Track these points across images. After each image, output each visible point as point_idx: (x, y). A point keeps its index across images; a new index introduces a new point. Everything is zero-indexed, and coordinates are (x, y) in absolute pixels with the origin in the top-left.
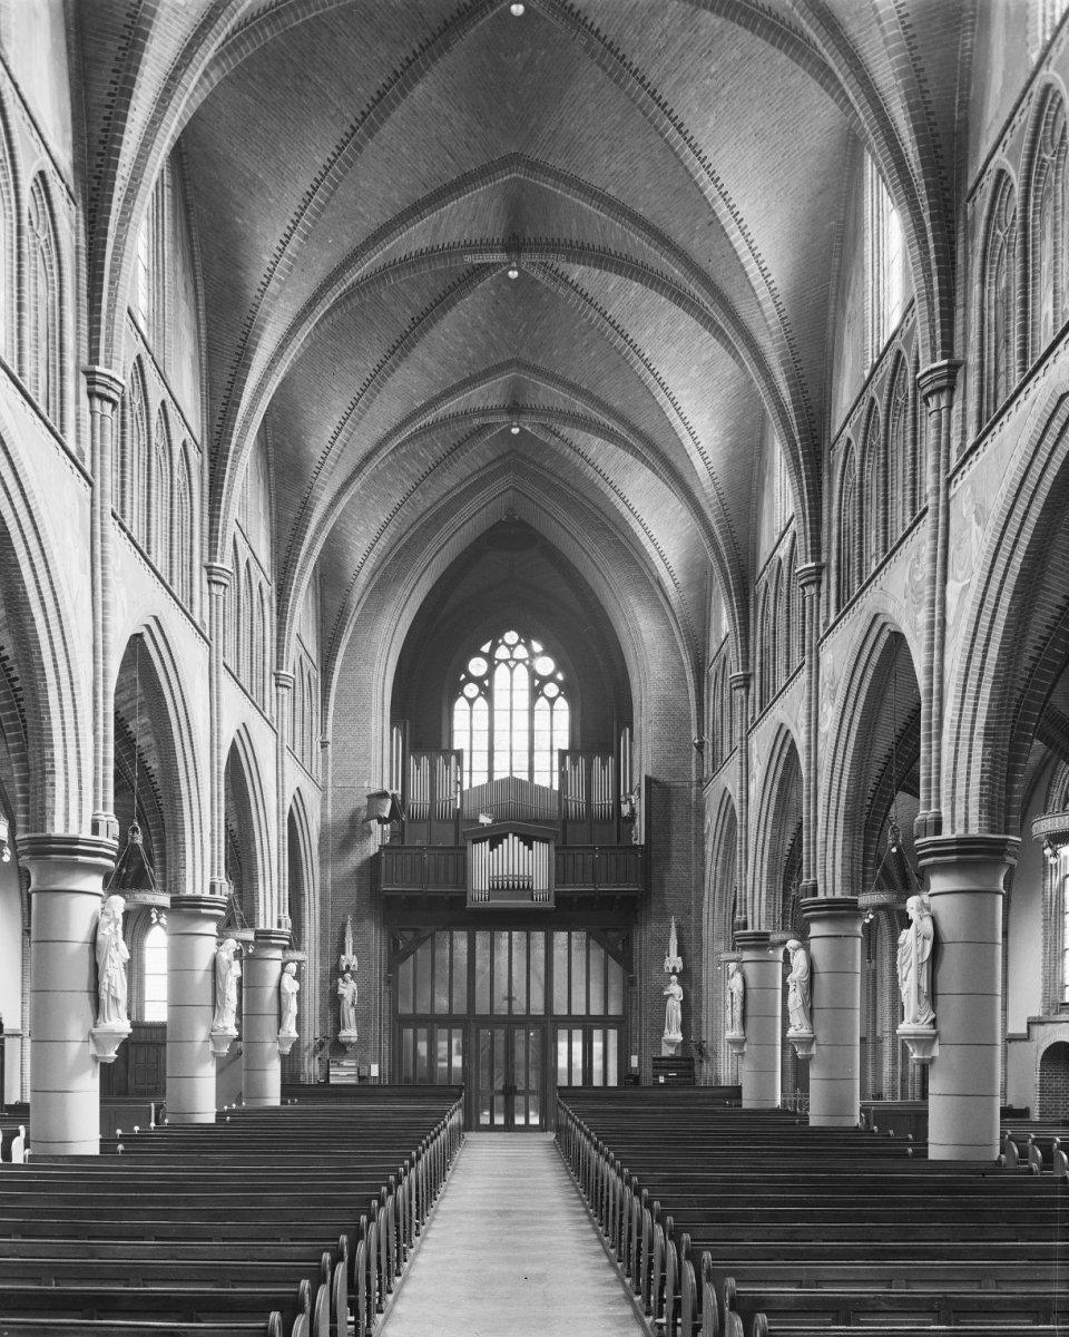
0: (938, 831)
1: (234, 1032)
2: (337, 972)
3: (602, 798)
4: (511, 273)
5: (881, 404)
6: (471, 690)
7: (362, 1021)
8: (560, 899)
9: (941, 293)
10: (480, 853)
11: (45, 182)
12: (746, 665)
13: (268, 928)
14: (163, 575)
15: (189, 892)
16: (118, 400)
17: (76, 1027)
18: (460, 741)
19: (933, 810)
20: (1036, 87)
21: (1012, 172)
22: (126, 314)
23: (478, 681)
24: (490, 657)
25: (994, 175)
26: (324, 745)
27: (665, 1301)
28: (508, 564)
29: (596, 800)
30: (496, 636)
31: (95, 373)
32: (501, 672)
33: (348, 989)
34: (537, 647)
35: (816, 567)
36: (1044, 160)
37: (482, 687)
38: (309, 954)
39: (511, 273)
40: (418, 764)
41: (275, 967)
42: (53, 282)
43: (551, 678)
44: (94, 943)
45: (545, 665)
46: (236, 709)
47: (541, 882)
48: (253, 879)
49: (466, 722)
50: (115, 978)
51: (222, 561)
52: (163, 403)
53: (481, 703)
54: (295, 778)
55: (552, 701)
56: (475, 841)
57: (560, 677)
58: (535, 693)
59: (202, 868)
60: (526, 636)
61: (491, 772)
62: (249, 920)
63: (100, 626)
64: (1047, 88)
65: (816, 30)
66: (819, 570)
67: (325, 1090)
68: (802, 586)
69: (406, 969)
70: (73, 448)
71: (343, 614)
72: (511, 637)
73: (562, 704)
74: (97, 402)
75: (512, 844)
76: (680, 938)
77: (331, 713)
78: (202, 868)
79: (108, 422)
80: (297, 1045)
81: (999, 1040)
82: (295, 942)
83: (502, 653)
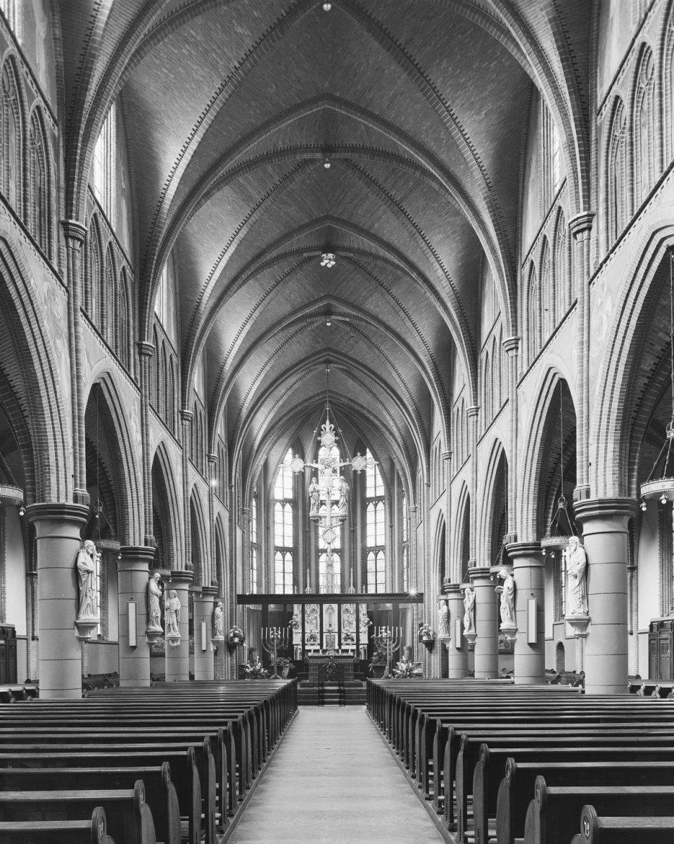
0: (516, 541)
4: (325, 6)
5: (537, 265)
9: (582, 171)
12: (476, 401)
13: (180, 570)
14: (97, 327)
16: (83, 239)
19: (585, 484)
21: (623, 96)
22: (87, 188)
25: (612, 99)
35: (587, 215)
36: (641, 88)
39: (325, 6)
42: (19, 127)
46: (158, 434)
48: (169, 539)
52: (110, 243)
63: (76, 378)
64: (644, 44)
65: (505, 16)
66: (477, 409)
68: (507, 351)
70: (56, 269)
74: (70, 240)
79: (77, 254)
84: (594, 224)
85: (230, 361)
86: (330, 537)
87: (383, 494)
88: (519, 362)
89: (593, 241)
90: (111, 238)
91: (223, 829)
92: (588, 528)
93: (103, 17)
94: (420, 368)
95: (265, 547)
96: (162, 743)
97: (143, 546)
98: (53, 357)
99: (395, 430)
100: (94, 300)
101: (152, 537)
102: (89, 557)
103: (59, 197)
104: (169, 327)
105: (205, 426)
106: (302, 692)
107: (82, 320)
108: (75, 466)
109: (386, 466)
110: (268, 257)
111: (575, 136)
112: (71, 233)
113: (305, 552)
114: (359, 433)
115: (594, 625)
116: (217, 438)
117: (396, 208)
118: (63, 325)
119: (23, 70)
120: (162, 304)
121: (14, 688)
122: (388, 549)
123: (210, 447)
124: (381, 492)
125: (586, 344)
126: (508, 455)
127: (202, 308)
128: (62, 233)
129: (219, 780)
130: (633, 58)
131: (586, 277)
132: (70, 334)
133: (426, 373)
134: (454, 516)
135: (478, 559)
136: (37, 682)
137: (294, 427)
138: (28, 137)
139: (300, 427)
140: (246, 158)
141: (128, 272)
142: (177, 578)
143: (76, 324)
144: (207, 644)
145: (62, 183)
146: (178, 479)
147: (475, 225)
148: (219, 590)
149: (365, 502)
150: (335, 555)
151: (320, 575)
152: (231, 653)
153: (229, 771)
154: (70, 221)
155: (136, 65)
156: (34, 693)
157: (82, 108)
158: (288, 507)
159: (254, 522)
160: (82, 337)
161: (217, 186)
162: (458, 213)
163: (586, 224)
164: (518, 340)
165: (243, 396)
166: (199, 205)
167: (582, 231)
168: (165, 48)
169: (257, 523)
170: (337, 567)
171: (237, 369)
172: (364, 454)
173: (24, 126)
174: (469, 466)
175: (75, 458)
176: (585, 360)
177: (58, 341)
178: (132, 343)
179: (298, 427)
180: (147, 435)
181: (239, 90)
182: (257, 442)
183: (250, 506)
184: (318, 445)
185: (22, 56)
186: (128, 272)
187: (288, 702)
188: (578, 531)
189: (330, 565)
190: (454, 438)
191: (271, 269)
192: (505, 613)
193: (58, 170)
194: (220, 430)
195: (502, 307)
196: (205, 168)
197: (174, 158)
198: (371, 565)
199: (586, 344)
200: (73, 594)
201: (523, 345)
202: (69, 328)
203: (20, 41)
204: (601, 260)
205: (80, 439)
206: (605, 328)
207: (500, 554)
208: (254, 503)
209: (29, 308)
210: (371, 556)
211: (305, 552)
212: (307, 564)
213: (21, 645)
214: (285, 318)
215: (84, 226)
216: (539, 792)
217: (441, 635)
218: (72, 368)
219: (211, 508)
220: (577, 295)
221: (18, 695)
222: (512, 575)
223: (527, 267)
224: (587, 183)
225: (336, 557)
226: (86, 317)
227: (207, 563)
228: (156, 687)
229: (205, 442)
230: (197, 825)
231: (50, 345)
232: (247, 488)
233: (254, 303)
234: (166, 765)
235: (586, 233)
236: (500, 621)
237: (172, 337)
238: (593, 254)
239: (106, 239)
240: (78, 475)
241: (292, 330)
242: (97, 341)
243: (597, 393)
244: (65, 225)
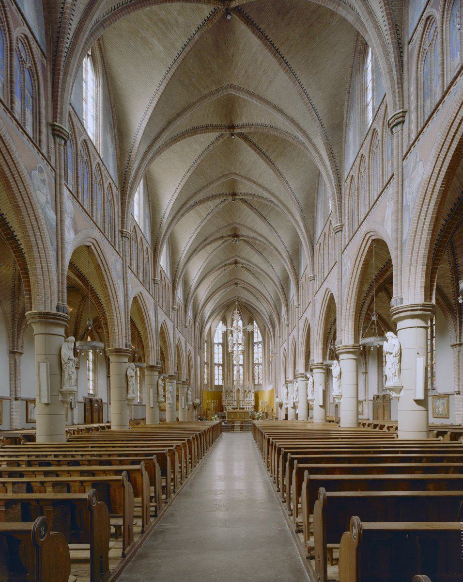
11: (86, 143)
16: (129, 237)
20: (360, 155)
27: (279, 477)
31: (122, 231)
35: (403, 112)
46: (162, 317)
51: (126, 229)
52: (141, 238)
54: (189, 347)
63: (126, 295)
70: (118, 250)
84: (343, 229)
85: (194, 285)
86: (239, 359)
87: (261, 340)
88: (315, 286)
89: (343, 235)
90: (141, 235)
91: (182, 482)
92: (341, 357)
93: (137, 145)
94: (275, 287)
95: (211, 364)
96: (158, 447)
97: (156, 365)
98: (117, 287)
99: (265, 313)
101: (159, 361)
102: (132, 370)
103: (119, 220)
104: (167, 271)
105: (183, 312)
106: (224, 426)
107: (129, 271)
108: (126, 332)
109: (262, 328)
110: (209, 240)
111: (335, 192)
112: (124, 235)
113: (228, 365)
114: (249, 314)
115: (421, 384)
116: (189, 318)
117: (263, 219)
118: (121, 274)
119: (103, 168)
120: (163, 261)
121: (102, 425)
122: (263, 364)
123: (185, 321)
124: (260, 339)
125: (340, 279)
126: (311, 325)
127: (181, 263)
128: (120, 235)
129: (180, 462)
130: (358, 160)
131: (340, 251)
132: (124, 277)
133: (278, 289)
134: (290, 350)
136: (110, 422)
137: (222, 313)
138: (106, 196)
139: (226, 311)
140: (199, 199)
142: (171, 377)
143: (126, 273)
144: (185, 405)
145: (120, 214)
146: (171, 336)
147: (296, 227)
148: (190, 383)
149: (253, 344)
150: (241, 367)
151: (234, 376)
152: (195, 409)
153: (186, 458)
154: (55, 123)
155: (151, 164)
156: (109, 427)
157: (128, 183)
158: (220, 346)
159: (206, 353)
160: (129, 279)
161: (187, 211)
162: (290, 221)
163: (340, 230)
164: (405, 112)
165: (200, 299)
166: (179, 220)
168: (165, 154)
169: (207, 353)
170: (241, 371)
171: (197, 288)
172: (252, 324)
173: (104, 192)
174: (295, 329)
175: (126, 329)
177: (118, 281)
178: (151, 279)
179: (225, 311)
180: (157, 317)
181: (198, 172)
182: (206, 319)
183: (204, 346)
184: (233, 320)
185: (103, 163)
186: (149, 249)
187: (215, 433)
188: (338, 358)
189: (238, 371)
190: (290, 317)
191: (211, 245)
192: (309, 393)
193: (118, 208)
194: (190, 314)
195: (308, 261)
196: (182, 204)
197: (168, 200)
198: (256, 371)
199: (340, 279)
200: (126, 386)
201: (317, 278)
202: (123, 275)
203: (102, 157)
204: (346, 244)
205: (128, 321)
206: (348, 272)
207: (308, 368)
208: (205, 345)
209: (106, 267)
210: (256, 367)
211: (228, 365)
212: (229, 371)
213: (105, 407)
214: (217, 266)
215: (129, 232)
216: (295, 466)
217: (284, 402)
218: (124, 291)
219: (186, 347)
220: (337, 259)
221: (103, 428)
222: (312, 376)
223: (318, 245)
224: (341, 214)
225: (241, 368)
226: (131, 269)
227: (184, 371)
228: (162, 424)
229: (183, 319)
230: (169, 480)
231: (115, 282)
232: (202, 340)
233: (204, 260)
234: (155, 456)
235: (340, 232)
236: (307, 396)
237: (169, 275)
238: (343, 242)
239: (139, 235)
240: (127, 336)
241: (221, 271)
242: (135, 279)
243: (345, 300)
244: (122, 232)
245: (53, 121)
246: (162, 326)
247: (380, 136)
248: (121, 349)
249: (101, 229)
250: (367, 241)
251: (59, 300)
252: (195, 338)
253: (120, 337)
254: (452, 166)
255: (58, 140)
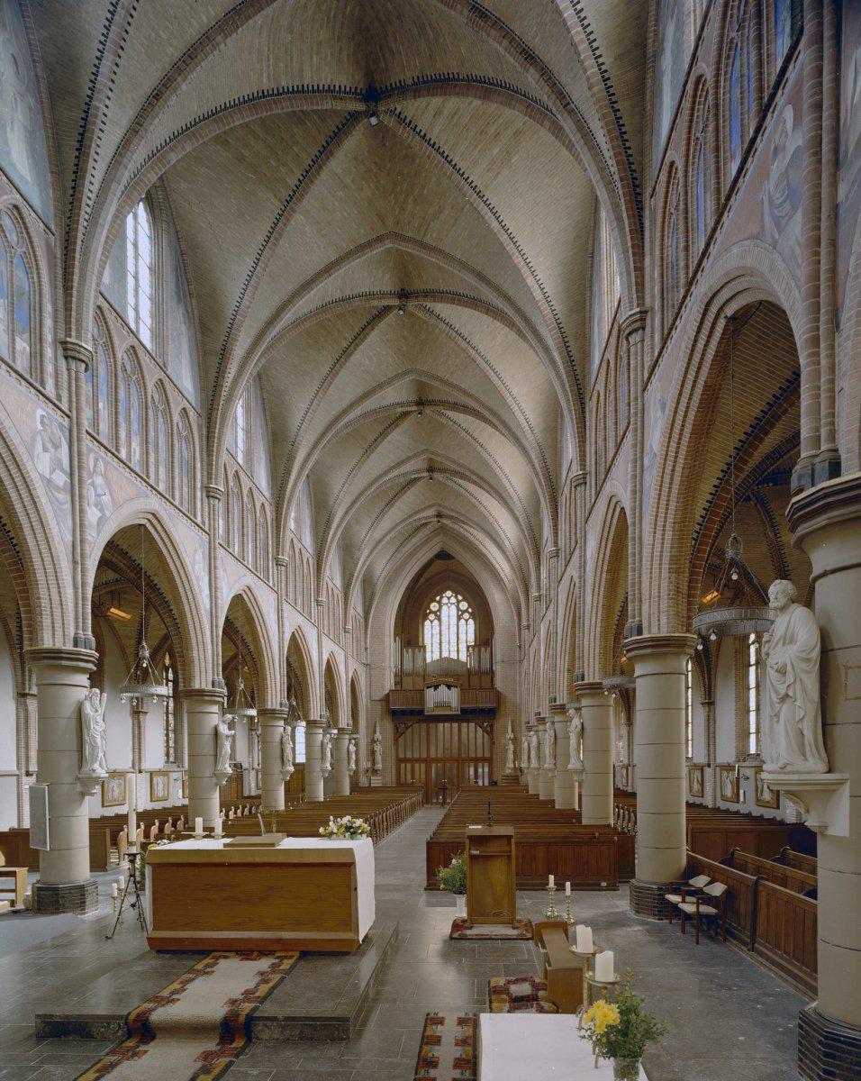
0: (555, 702)
1: (330, 768)
2: (373, 741)
3: (485, 665)
6: (432, 617)
7: (384, 761)
8: (463, 711)
10: (430, 693)
15: (312, 718)
17: (276, 768)
18: (427, 642)
23: (435, 613)
24: (439, 602)
26: (366, 649)
28: (444, 572)
29: (483, 666)
30: (441, 593)
31: (66, 342)
32: (445, 608)
33: (378, 748)
34: (460, 598)
35: (641, 312)
37: (436, 615)
38: (362, 736)
40: (407, 651)
41: (346, 742)
43: (466, 611)
44: (282, 743)
45: (464, 605)
47: (455, 704)
48: (337, 708)
49: (429, 630)
50: (288, 751)
53: (436, 622)
55: (467, 621)
56: (428, 688)
57: (470, 610)
58: (459, 618)
59: (317, 708)
60: (456, 592)
61: (441, 652)
62: (336, 725)
67: (370, 789)
69: (401, 740)
71: (373, 595)
72: (449, 593)
73: (471, 622)
75: (443, 688)
76: (512, 726)
77: (369, 632)
78: (317, 708)
80: (356, 772)
81: (685, 771)
82: (355, 729)
83: (445, 600)
89: (647, 341)
97: (210, 688)
100: (552, 830)
135: (586, 670)
141: (268, 508)
154: (68, 339)
164: (646, 312)
167: (636, 330)
176: (637, 493)
235: (640, 332)
245: (66, 336)
246: (328, 661)
247: (680, 174)
248: (60, 651)
249: (110, 448)
250: (713, 327)
251: (213, 675)
252: (366, 649)
253: (207, 669)
254: (705, 403)
255: (73, 364)
